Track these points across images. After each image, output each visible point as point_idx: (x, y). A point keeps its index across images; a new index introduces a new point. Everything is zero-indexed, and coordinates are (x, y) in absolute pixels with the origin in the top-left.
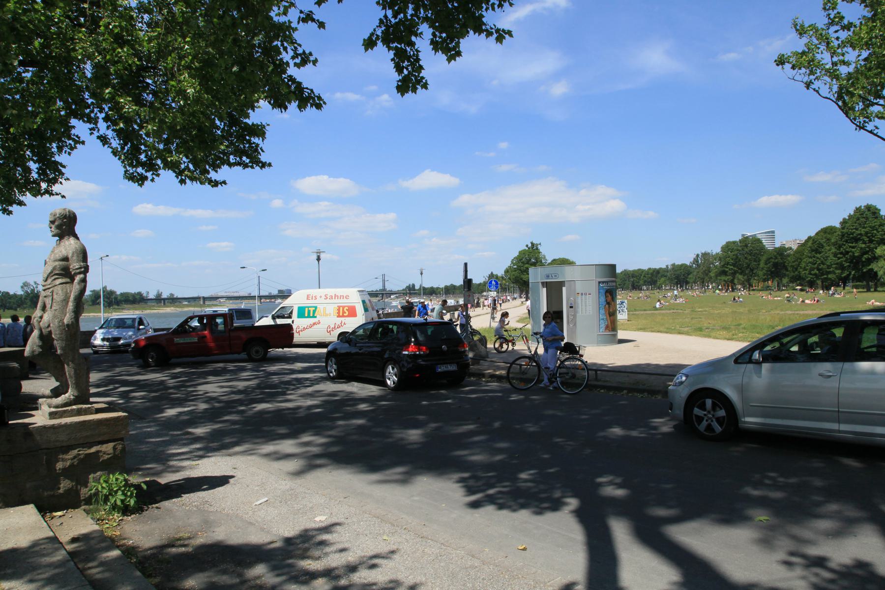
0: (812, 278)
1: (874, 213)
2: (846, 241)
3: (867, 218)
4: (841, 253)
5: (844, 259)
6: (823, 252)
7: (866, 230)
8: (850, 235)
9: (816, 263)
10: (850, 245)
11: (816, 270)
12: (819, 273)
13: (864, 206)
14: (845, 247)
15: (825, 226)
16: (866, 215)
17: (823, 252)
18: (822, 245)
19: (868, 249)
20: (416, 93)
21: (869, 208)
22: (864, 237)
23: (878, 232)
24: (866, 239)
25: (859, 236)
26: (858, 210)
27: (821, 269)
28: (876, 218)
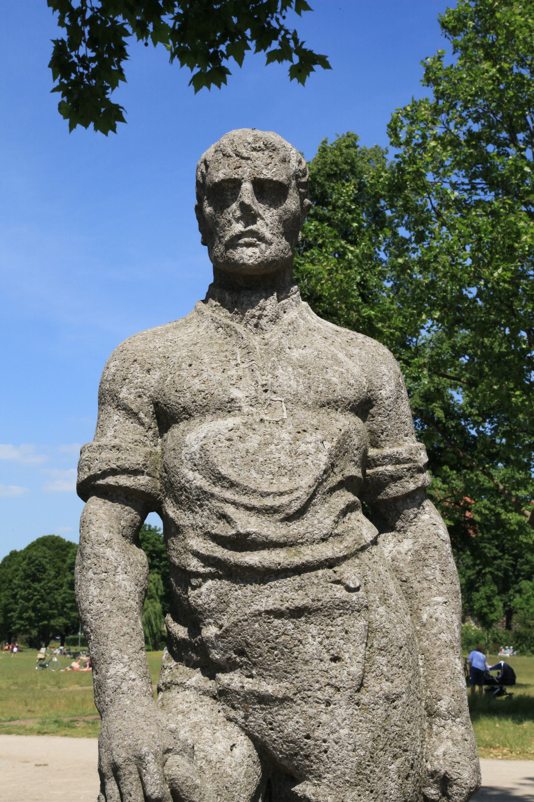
0: (22, 625)
6: (44, 579)
9: (32, 599)
11: (30, 611)
12: (36, 616)
17: (44, 579)
18: (44, 567)
20: (197, 90)
27: (39, 610)
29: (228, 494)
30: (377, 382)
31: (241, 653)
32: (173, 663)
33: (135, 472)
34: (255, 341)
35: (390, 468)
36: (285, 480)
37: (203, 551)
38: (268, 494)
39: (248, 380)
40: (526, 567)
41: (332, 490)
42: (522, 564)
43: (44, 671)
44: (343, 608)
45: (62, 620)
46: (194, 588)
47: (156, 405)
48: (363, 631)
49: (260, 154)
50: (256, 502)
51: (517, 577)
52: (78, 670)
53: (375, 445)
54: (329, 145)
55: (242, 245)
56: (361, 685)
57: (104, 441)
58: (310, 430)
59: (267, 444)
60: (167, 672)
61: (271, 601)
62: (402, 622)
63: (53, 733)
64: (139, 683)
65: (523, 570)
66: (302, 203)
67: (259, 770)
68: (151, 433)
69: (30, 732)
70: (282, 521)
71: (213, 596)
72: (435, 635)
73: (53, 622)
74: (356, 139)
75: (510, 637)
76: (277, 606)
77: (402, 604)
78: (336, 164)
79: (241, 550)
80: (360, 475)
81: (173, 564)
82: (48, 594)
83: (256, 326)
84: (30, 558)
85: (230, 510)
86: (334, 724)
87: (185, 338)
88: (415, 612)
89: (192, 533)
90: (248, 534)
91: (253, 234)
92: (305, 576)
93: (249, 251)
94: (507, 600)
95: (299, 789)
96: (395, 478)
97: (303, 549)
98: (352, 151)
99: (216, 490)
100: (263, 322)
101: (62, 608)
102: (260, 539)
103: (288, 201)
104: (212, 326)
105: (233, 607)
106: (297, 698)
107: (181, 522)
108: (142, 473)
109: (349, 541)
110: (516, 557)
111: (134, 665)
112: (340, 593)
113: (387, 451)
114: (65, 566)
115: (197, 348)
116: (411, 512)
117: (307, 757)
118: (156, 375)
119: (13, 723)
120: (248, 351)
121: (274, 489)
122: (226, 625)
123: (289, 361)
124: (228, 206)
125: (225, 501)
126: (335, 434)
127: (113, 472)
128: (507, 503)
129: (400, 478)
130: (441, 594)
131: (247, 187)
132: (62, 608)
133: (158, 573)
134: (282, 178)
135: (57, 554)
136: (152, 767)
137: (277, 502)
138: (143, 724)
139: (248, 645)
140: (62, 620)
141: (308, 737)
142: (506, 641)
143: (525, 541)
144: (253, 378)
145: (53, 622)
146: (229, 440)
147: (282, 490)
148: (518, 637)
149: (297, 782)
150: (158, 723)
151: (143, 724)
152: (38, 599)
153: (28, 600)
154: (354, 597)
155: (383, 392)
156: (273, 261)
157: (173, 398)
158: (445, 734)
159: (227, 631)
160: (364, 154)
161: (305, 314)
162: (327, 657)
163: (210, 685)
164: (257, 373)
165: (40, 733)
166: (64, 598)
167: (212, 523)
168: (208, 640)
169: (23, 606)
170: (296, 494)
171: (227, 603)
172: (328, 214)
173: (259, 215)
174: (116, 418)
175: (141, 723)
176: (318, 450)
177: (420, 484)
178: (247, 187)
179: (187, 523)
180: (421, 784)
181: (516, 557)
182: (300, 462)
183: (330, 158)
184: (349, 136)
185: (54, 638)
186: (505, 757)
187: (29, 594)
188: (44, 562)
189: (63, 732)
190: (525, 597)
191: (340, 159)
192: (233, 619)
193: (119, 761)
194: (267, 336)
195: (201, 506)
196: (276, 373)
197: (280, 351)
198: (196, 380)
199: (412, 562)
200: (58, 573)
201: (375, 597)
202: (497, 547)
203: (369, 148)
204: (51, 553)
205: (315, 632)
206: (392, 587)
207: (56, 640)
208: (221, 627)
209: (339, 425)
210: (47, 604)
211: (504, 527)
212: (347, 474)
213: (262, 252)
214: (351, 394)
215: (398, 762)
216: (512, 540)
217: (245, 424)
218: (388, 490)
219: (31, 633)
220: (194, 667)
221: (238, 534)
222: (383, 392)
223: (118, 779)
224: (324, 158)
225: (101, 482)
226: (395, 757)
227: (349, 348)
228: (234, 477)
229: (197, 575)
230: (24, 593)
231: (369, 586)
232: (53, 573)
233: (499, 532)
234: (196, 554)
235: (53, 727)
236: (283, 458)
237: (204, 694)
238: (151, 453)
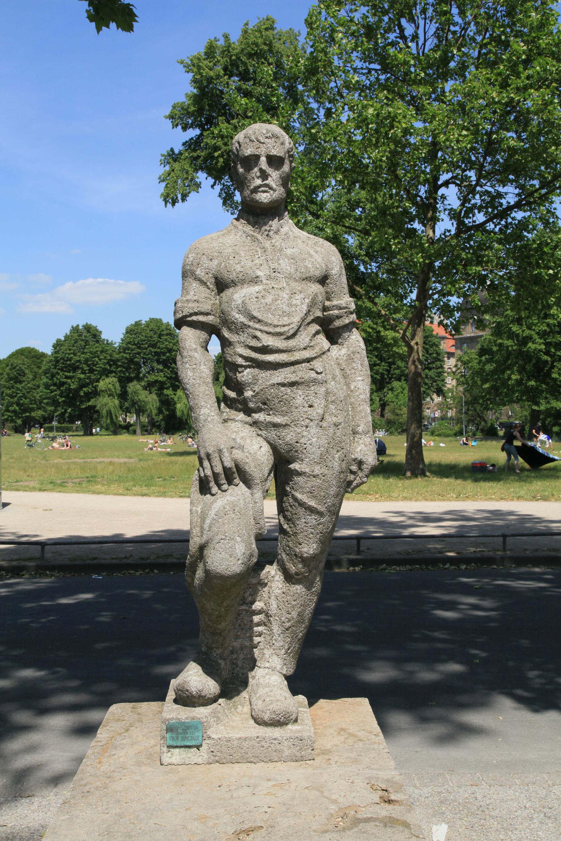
0: (9, 416)
1: (95, 336)
2: (62, 370)
3: (87, 342)
4: (55, 385)
5: (58, 392)
6: (24, 381)
7: (86, 356)
8: (67, 361)
9: (16, 396)
10: (67, 374)
11: (15, 406)
12: (20, 409)
13: (83, 326)
14: (59, 377)
15: (19, 348)
16: (85, 337)
17: (24, 381)
18: (23, 372)
19: (87, 381)
21: (88, 328)
22: (84, 366)
23: (100, 360)
24: (86, 368)
25: (78, 364)
26: (75, 329)
27: (22, 405)
28: (97, 342)
29: (257, 326)
30: (330, 266)
31: (265, 404)
32: (228, 410)
33: (207, 314)
34: (267, 244)
35: (336, 312)
36: (286, 318)
37: (245, 354)
38: (278, 326)
39: (265, 266)
40: (397, 372)
41: (309, 324)
42: (395, 369)
43: (31, 449)
44: (314, 382)
45: (40, 413)
46: (240, 373)
47: (216, 278)
48: (323, 393)
49: (270, 140)
50: (271, 330)
51: (390, 379)
52: (57, 449)
53: (328, 299)
54: (250, 27)
55: (260, 192)
56: (323, 418)
57: (189, 297)
58: (298, 293)
59: (276, 300)
60: (225, 414)
61: (280, 378)
62: (342, 389)
63: (51, 490)
64: (216, 417)
65: (395, 374)
66: (291, 166)
67: (273, 458)
68: (213, 293)
69: (34, 489)
70: (285, 339)
71: (250, 377)
72: (357, 396)
73: (33, 414)
74: (273, 22)
75: (383, 422)
76: (283, 381)
77: (342, 380)
78: (256, 44)
79: (264, 354)
80: (322, 316)
81: (228, 361)
82: (28, 392)
83: (267, 235)
84: (12, 365)
85: (258, 334)
86: (309, 436)
87: (229, 241)
88: (348, 385)
89: (238, 345)
90: (268, 346)
91: (267, 185)
92: (296, 366)
93: (265, 195)
94: (382, 396)
95: (292, 466)
96: (339, 317)
97: (295, 353)
98: (269, 33)
99: (251, 324)
100: (271, 233)
101: (40, 403)
102: (274, 348)
103: (284, 166)
104: (244, 235)
105: (260, 381)
106: (292, 425)
107: (232, 340)
108: (210, 314)
109: (317, 349)
110: (390, 364)
111: (212, 409)
112: (313, 375)
113: (335, 303)
114: (40, 371)
115: (237, 248)
116: (346, 335)
117: (296, 451)
118: (215, 262)
119: (18, 484)
120: (265, 250)
121: (280, 323)
122: (257, 390)
123: (286, 255)
124: (252, 169)
125: (256, 329)
126: (310, 295)
127: (196, 314)
128: (386, 323)
129: (341, 317)
130: (361, 376)
131: (263, 159)
132: (40, 403)
133: (115, 377)
134: (281, 154)
135: (33, 362)
136: (226, 454)
137: (282, 330)
138: (220, 436)
139: (268, 400)
140: (40, 413)
141: (297, 442)
142: (380, 425)
143: (397, 351)
144: (268, 265)
145: (33, 414)
146: (257, 298)
147: (285, 323)
148: (389, 423)
149: (291, 463)
150: (227, 435)
151: (220, 436)
152: (21, 397)
153: (12, 397)
154: (320, 376)
155: (333, 271)
156: (277, 200)
157: (226, 275)
158: (361, 442)
159: (257, 393)
160: (280, 35)
161: (292, 228)
162: (306, 405)
163: (248, 419)
164: (270, 262)
165: (40, 490)
166: (41, 396)
167: (249, 340)
168: (248, 398)
169: (9, 402)
170: (292, 326)
171: (258, 380)
172: (250, 89)
173: (270, 175)
174: (194, 285)
175: (219, 435)
176: (302, 303)
177: (351, 320)
178: (263, 159)
179: (236, 340)
180: (349, 464)
181: (390, 364)
182: (293, 309)
183: (252, 39)
184: (268, 19)
185: (34, 426)
186: (377, 500)
187: (13, 392)
188: (23, 368)
189: (58, 490)
190: (395, 393)
191: (260, 41)
192: (261, 388)
193: (210, 452)
194: (273, 241)
195: (243, 332)
196: (280, 262)
197: (281, 250)
198: (238, 266)
199: (347, 360)
200: (35, 377)
201: (329, 377)
202: (377, 356)
203: (284, 30)
204: (29, 361)
205: (301, 394)
206: (337, 372)
207: (35, 427)
208: (254, 391)
209: (312, 290)
210: (28, 400)
211: (383, 342)
212: (316, 315)
213: (271, 196)
214: (318, 274)
215: (339, 454)
216: (389, 351)
217: (264, 289)
218: (335, 323)
219: (15, 422)
220: (239, 411)
221: (263, 346)
222: (333, 271)
223: (209, 460)
224: (246, 39)
225: (189, 319)
226: (338, 451)
227: (316, 247)
228: (260, 317)
229: (242, 366)
230: (9, 392)
231: (327, 371)
232: (31, 376)
233: (378, 346)
234: (241, 356)
235: (50, 486)
236: (285, 307)
237: (245, 423)
238: (214, 304)
